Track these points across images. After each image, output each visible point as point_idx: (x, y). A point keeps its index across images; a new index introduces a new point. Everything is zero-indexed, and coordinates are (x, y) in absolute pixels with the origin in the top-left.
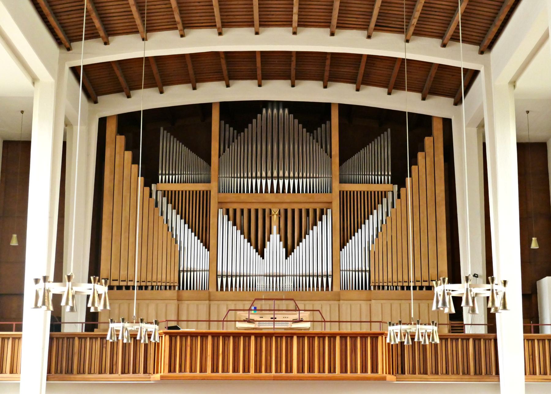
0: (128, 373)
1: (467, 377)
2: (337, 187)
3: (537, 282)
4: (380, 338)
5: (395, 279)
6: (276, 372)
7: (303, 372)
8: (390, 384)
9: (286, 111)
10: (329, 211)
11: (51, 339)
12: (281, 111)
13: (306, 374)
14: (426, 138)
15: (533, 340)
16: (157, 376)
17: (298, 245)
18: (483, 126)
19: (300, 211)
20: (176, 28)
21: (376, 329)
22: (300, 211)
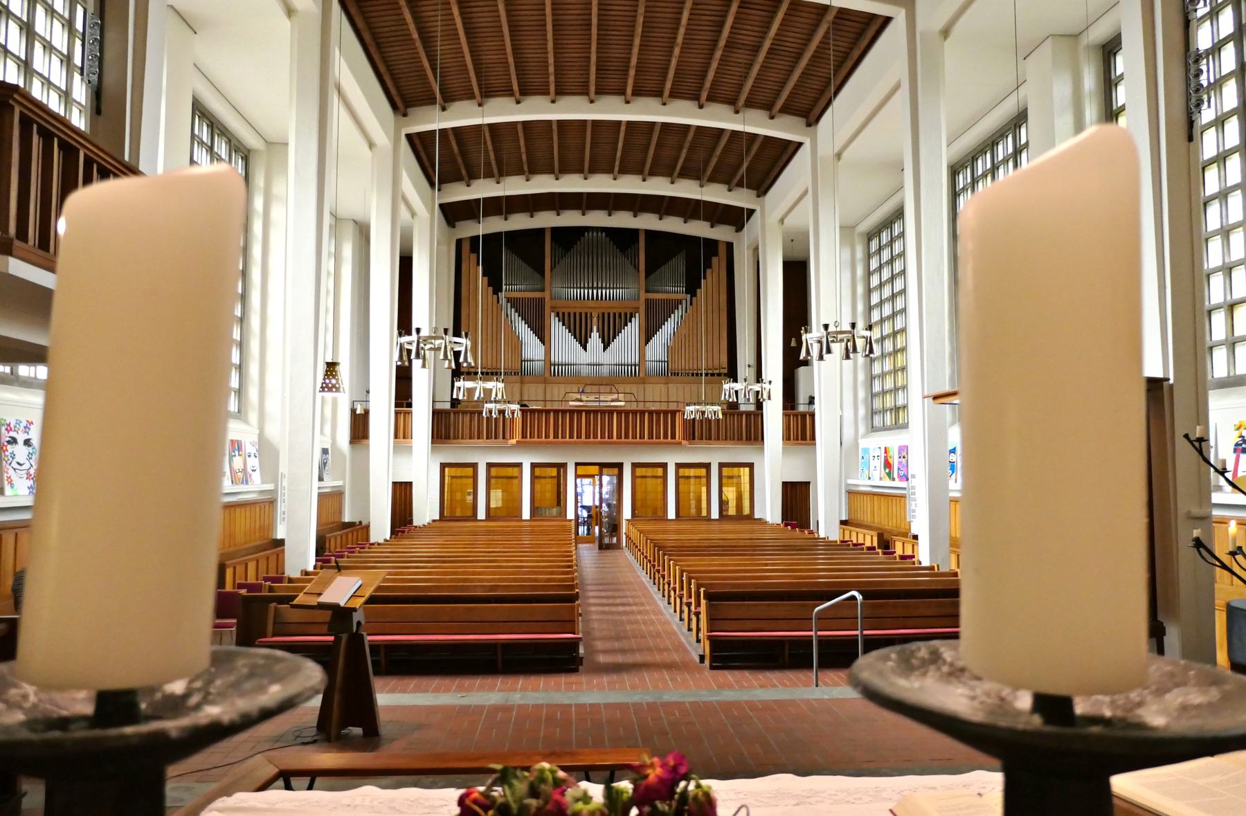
0: (491, 438)
1: (741, 442)
2: (643, 296)
3: (795, 370)
4: (678, 414)
5: (687, 368)
6: (601, 438)
7: (621, 438)
9: (604, 233)
10: (637, 315)
11: (397, 413)
12: (600, 234)
13: (560, 439)
14: (713, 258)
15: (789, 416)
16: (514, 441)
17: (613, 341)
18: (758, 249)
19: (615, 314)
20: (524, 174)
21: (673, 407)
22: (615, 314)
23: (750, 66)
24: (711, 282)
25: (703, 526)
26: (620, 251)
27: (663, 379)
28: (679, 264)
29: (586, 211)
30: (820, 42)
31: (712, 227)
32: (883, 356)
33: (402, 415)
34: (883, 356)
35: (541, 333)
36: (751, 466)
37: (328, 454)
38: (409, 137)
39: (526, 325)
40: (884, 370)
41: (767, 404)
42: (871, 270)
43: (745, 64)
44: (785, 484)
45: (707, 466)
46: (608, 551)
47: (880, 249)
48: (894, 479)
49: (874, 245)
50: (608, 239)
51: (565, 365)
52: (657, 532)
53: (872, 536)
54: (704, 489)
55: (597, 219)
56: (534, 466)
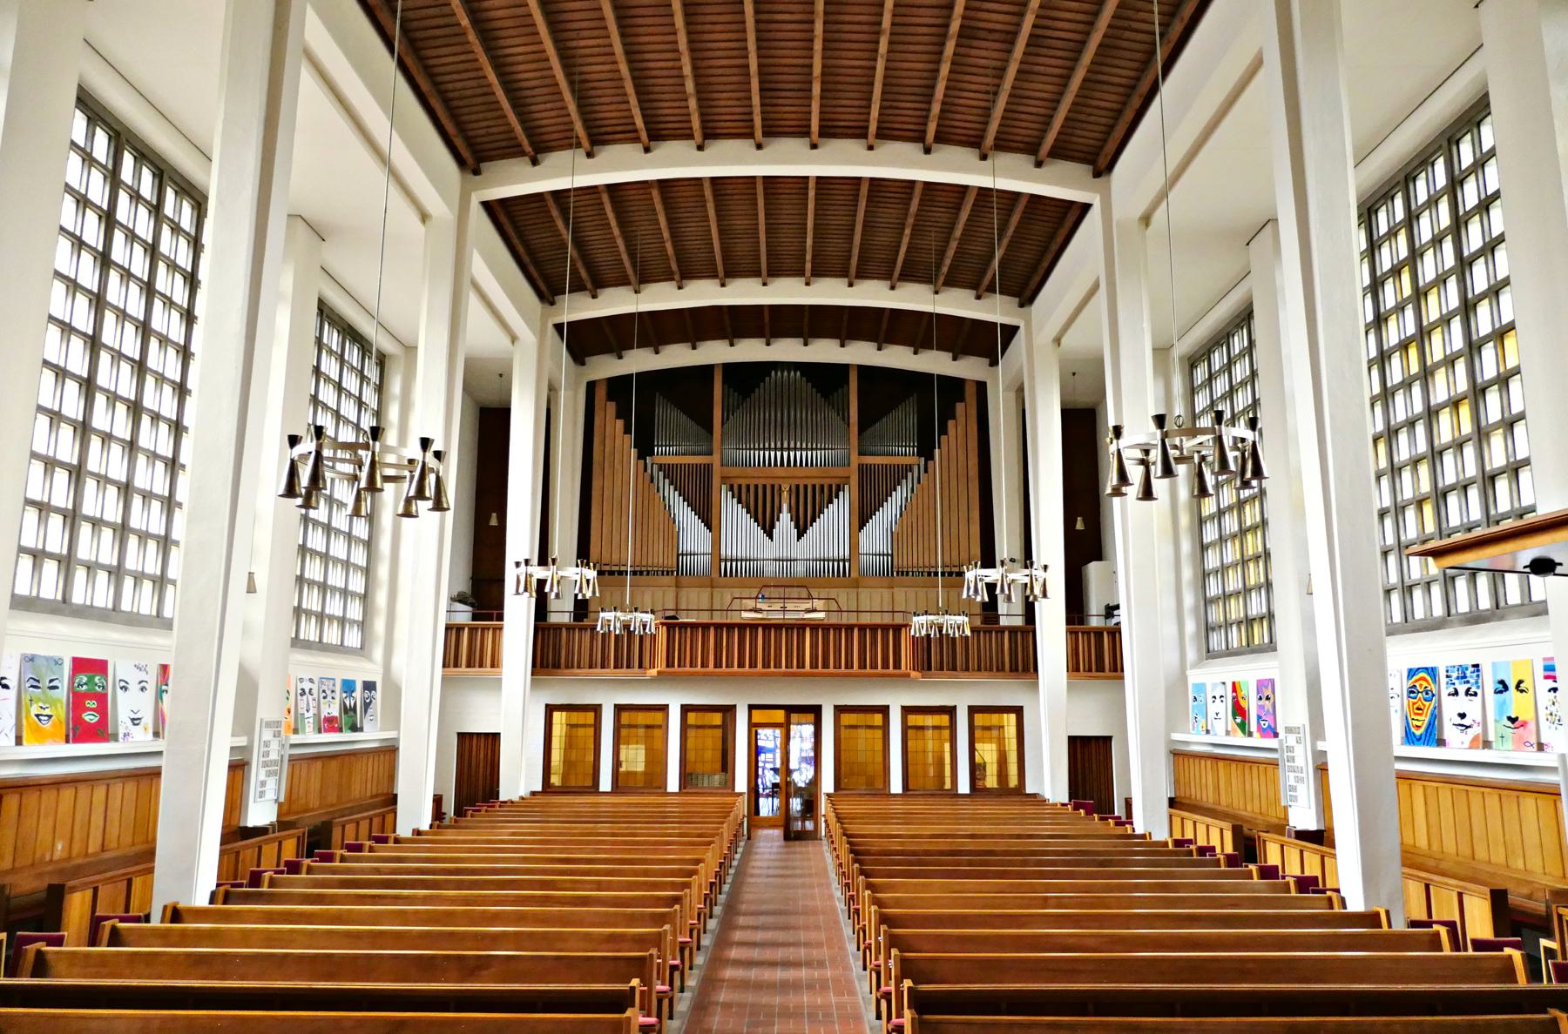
0: (622, 667)
1: (967, 673)
2: (855, 460)
4: (903, 629)
6: (787, 667)
7: (817, 667)
8: (915, 680)
9: (798, 373)
10: (847, 487)
15: (1076, 633)
16: (654, 672)
17: (812, 525)
19: (814, 486)
20: (673, 279)
21: (899, 620)
23: (1002, 71)
24: (956, 439)
25: (945, 807)
26: (822, 396)
27: (886, 581)
28: (906, 417)
29: (772, 340)
30: (1113, 17)
31: (955, 359)
32: (1222, 540)
33: (491, 632)
34: (1222, 540)
35: (707, 516)
36: (1018, 711)
37: (375, 690)
38: (487, 206)
39: (686, 503)
40: (1225, 562)
41: (1040, 607)
42: (1197, 411)
43: (994, 68)
44: (1073, 740)
45: (951, 711)
46: (797, 843)
47: (1211, 378)
48: (1250, 734)
49: (1201, 374)
50: (804, 379)
51: (737, 560)
52: (867, 818)
53: (1222, 830)
54: (947, 746)
55: (788, 350)
56: (686, 709)
